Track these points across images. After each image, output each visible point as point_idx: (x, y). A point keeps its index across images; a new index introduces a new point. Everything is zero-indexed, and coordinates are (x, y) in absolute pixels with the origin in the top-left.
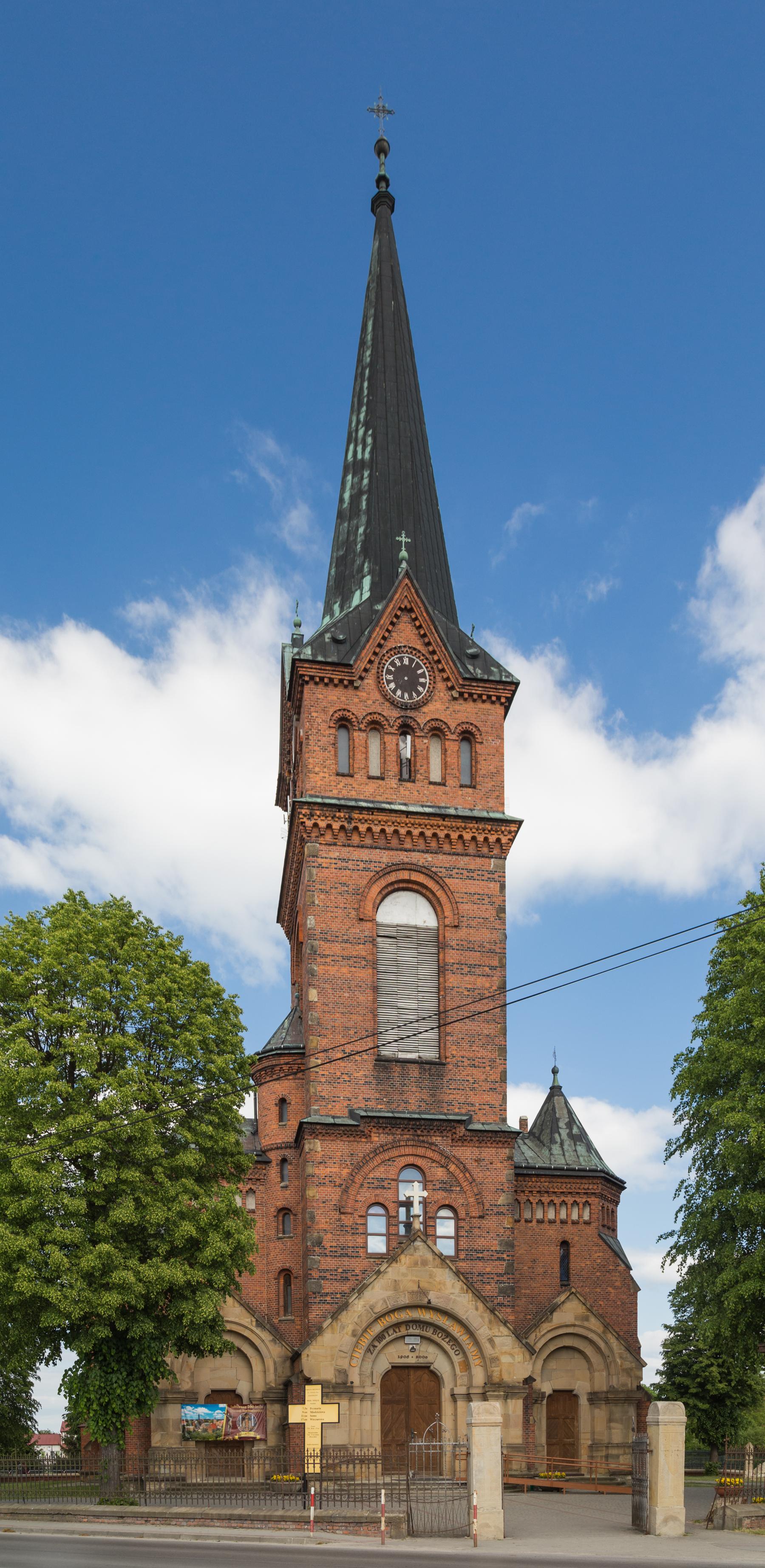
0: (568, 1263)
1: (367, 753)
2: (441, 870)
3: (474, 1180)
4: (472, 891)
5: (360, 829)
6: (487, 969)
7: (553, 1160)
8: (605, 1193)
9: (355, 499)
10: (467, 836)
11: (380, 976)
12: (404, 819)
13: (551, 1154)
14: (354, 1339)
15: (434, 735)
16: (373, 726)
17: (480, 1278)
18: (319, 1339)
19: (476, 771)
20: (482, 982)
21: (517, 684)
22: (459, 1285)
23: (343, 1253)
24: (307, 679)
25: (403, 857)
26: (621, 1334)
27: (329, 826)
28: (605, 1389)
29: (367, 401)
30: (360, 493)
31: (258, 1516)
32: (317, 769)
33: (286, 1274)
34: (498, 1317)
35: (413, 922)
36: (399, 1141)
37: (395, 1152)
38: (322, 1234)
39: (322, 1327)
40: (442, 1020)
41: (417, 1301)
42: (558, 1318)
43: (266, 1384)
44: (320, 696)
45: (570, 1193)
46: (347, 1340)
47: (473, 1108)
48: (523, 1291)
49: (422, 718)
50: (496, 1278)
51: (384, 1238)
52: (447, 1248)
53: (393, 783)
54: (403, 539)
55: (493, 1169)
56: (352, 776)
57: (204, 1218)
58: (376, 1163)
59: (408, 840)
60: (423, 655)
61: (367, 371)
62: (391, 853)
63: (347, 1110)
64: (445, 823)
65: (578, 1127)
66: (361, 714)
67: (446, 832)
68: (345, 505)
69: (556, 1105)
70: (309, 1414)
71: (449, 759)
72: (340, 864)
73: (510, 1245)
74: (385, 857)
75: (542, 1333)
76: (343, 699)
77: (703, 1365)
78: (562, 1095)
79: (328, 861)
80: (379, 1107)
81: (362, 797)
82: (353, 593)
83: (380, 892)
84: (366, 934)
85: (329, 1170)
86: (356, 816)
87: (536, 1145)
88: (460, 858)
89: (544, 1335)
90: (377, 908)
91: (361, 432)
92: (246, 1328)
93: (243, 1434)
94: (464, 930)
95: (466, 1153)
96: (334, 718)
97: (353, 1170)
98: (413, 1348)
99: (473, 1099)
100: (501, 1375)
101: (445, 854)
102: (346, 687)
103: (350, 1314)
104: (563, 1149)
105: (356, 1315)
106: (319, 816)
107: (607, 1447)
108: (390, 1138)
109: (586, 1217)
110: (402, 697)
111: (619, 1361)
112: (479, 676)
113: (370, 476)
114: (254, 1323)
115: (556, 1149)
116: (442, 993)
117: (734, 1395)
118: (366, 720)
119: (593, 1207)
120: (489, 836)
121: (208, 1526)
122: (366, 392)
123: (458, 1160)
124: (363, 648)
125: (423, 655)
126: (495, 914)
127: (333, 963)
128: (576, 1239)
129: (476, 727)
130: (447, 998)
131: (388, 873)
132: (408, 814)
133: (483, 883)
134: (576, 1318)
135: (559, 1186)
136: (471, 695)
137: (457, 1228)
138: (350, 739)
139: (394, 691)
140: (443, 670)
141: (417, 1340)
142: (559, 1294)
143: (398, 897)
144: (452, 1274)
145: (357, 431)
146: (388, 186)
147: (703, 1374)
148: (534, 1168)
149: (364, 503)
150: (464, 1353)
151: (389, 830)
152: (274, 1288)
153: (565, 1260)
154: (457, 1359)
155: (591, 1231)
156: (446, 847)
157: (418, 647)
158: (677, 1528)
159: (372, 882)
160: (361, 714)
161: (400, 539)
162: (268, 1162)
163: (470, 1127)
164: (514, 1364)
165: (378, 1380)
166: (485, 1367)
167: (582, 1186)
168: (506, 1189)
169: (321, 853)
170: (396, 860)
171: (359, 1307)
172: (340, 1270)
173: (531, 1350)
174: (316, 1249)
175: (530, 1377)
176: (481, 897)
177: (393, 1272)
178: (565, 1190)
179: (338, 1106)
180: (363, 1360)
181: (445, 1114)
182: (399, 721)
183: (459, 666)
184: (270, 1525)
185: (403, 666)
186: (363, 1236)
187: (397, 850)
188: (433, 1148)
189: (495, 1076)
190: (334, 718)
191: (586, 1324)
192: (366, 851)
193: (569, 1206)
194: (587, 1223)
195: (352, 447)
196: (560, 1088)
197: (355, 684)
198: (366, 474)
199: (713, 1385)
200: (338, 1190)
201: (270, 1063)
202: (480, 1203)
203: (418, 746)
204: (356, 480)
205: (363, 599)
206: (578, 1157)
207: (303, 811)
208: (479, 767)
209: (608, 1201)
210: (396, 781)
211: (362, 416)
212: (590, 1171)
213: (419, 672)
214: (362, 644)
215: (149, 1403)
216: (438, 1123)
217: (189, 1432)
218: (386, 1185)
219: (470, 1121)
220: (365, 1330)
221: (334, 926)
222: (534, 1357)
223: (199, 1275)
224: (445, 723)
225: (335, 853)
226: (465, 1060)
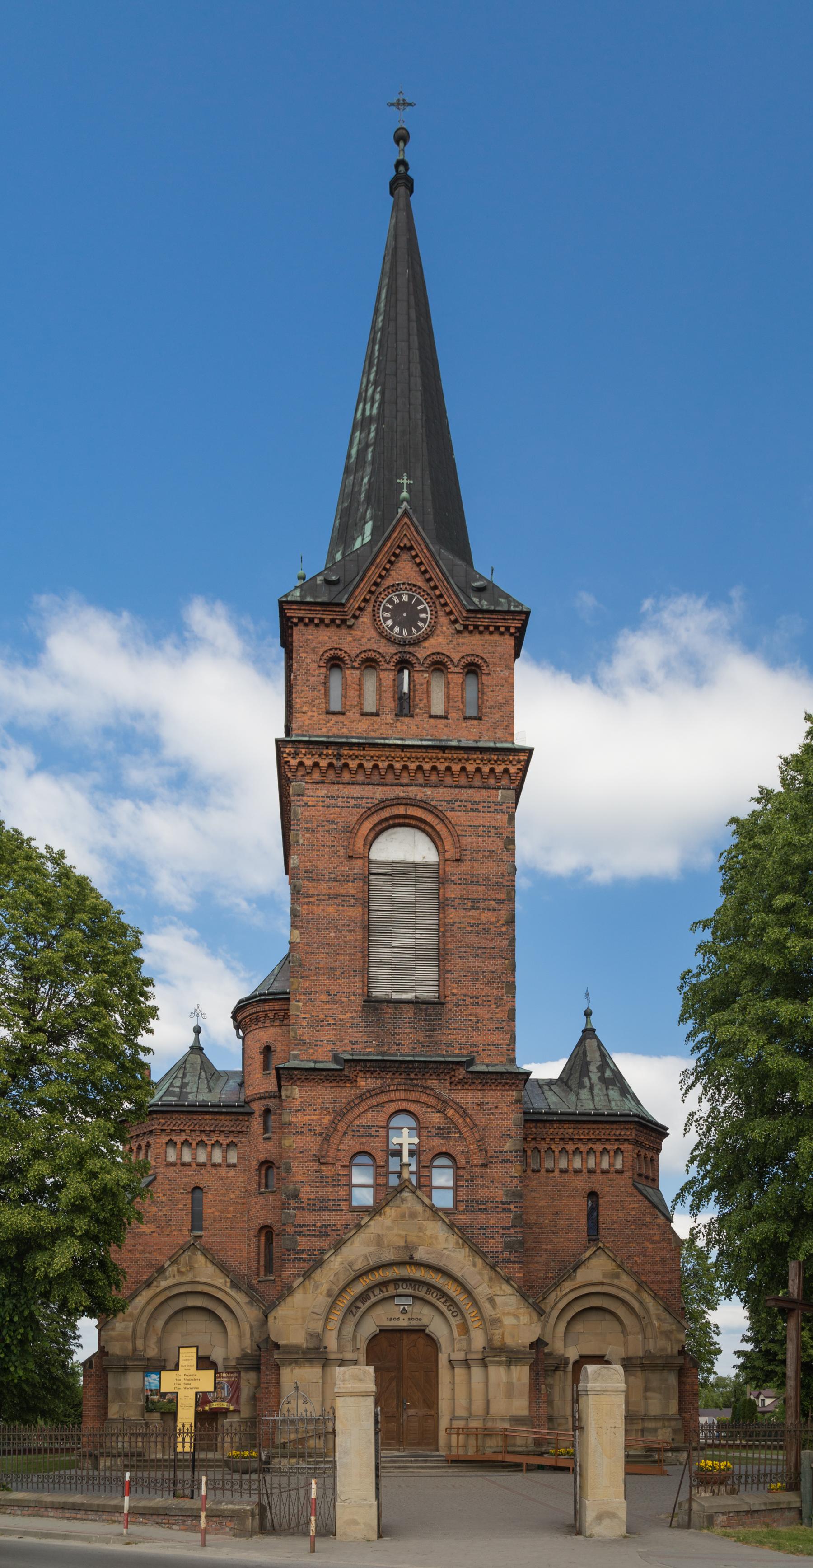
0: (598, 1215)
1: (361, 690)
2: (441, 803)
3: (476, 1125)
4: (477, 823)
5: (351, 766)
6: (493, 903)
7: (579, 1104)
8: (641, 1139)
9: (362, 453)
10: (471, 768)
12: (399, 753)
13: (578, 1099)
14: (330, 1300)
15: (436, 670)
16: (368, 663)
17: (482, 1232)
18: (289, 1299)
19: (483, 703)
20: (486, 916)
21: (527, 614)
22: (453, 1239)
23: (321, 1206)
24: (295, 620)
25: (399, 792)
26: (661, 1292)
27: (316, 765)
29: (378, 362)
30: (367, 446)
31: (91, 1505)
32: (305, 709)
33: (267, 1231)
34: (500, 1274)
35: (410, 858)
36: (389, 1085)
37: (384, 1098)
39: (291, 1287)
40: (441, 957)
42: (582, 1276)
43: (243, 1350)
44: (310, 637)
45: (599, 1140)
48: (544, 1247)
51: (372, 1189)
52: (443, 1200)
53: (390, 718)
54: (405, 481)
55: (500, 1115)
57: (64, 1155)
58: (362, 1110)
60: (424, 591)
61: (379, 335)
62: (386, 788)
63: (330, 1054)
64: (445, 755)
65: (612, 1070)
67: (446, 764)
68: (352, 460)
69: (588, 1048)
71: (451, 692)
72: (328, 802)
73: (518, 1195)
74: (379, 793)
75: (564, 1292)
78: (596, 1038)
80: (368, 1050)
81: (354, 734)
84: (356, 871)
85: (307, 1117)
86: (346, 752)
89: (566, 1295)
91: (370, 391)
92: (220, 1289)
93: (215, 1405)
94: (467, 863)
95: (467, 1097)
96: (325, 657)
97: (335, 1118)
98: (404, 1309)
100: (503, 1338)
101: (445, 787)
102: (338, 626)
103: (325, 1272)
104: (592, 1093)
106: (305, 755)
108: (379, 1083)
112: (485, 608)
113: (377, 429)
114: (229, 1284)
116: (441, 930)
118: (360, 658)
120: (495, 766)
121: (42, 1516)
122: (376, 354)
123: (457, 1104)
125: (424, 591)
126: (502, 845)
127: (318, 902)
129: (482, 658)
130: (447, 935)
131: (382, 809)
132: (403, 747)
133: (489, 815)
134: (604, 1276)
135: (584, 1133)
137: (456, 1178)
138: (344, 678)
141: (410, 1300)
143: (394, 833)
144: (445, 1228)
145: (366, 390)
146: (407, 169)
148: (556, 1114)
150: (462, 1314)
151: (383, 765)
152: (254, 1247)
153: (593, 1214)
154: (454, 1321)
155: (625, 1180)
156: (448, 780)
157: (419, 584)
158: (614, 1528)
159: (363, 819)
161: (401, 481)
162: (251, 1114)
163: (471, 1069)
164: (518, 1325)
165: (362, 1345)
166: (485, 1329)
167: (613, 1132)
168: (513, 1134)
169: (307, 791)
170: (390, 796)
171: (336, 1266)
172: (319, 1225)
173: (541, 1313)
174: (292, 1202)
175: (539, 1340)
176: (487, 829)
177: (375, 1226)
178: (592, 1137)
179: (321, 1050)
180: (342, 1323)
181: (444, 1056)
182: (397, 657)
183: (462, 598)
184: (104, 1517)
185: (402, 602)
186: (346, 1188)
187: (392, 785)
189: (501, 1014)
190: (325, 657)
191: (616, 1282)
192: (358, 787)
193: (598, 1154)
194: (619, 1172)
195: (361, 406)
196: (594, 1030)
198: (373, 428)
201: (254, 1010)
204: (363, 435)
205: (365, 542)
206: (610, 1101)
207: (287, 750)
208: (485, 698)
209: (644, 1147)
210: (393, 716)
211: (372, 377)
212: (622, 1115)
213: (420, 607)
215: (12, 1369)
216: (434, 1065)
217: (153, 1403)
219: (471, 1062)
221: (321, 865)
222: (542, 1318)
223: (49, 1222)
224: (448, 657)
225: (323, 791)
226: (467, 998)
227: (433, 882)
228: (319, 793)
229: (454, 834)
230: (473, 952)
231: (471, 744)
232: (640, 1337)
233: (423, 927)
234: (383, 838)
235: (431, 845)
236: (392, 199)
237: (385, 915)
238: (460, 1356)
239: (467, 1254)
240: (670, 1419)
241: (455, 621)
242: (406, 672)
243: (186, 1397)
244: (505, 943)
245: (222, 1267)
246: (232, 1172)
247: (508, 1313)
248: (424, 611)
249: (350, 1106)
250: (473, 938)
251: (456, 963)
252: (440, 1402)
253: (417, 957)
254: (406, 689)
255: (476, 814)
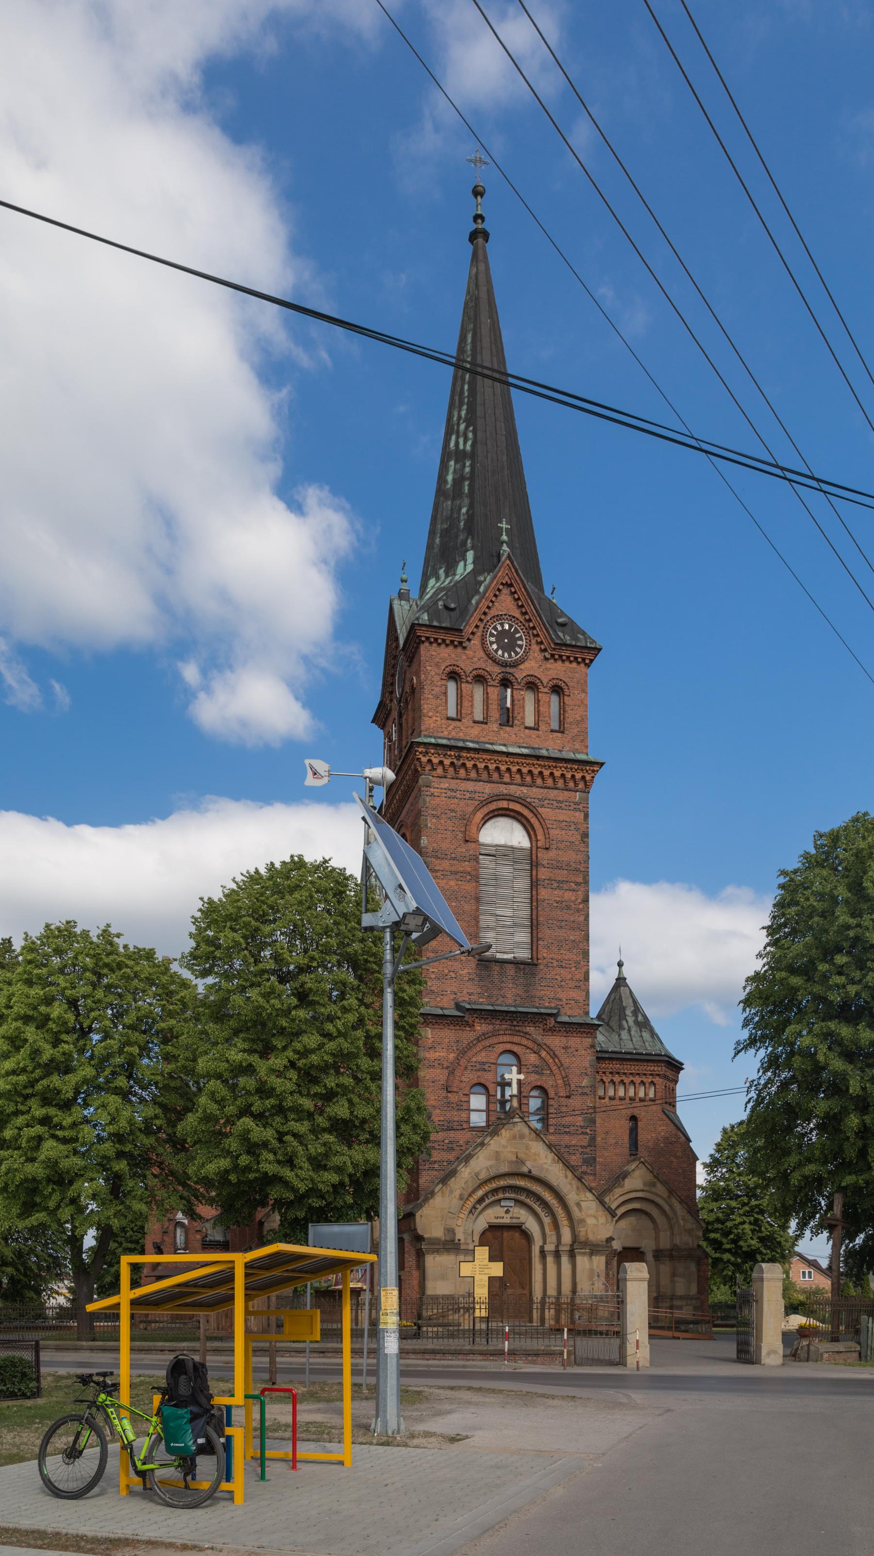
1: (472, 701)
3: (562, 1065)
4: (561, 819)
6: (573, 885)
7: (622, 1044)
9: (458, 482)
10: (557, 774)
11: (481, 888)
14: (461, 1202)
17: (567, 1150)
18: (431, 1201)
19: (564, 719)
22: (551, 1156)
24: (423, 639)
26: (683, 1198)
27: (441, 762)
28: (668, 1247)
29: (468, 401)
32: (430, 714)
36: (498, 1030)
37: (494, 1040)
40: (534, 926)
41: (514, 1169)
44: (434, 653)
45: (638, 1074)
46: (456, 1202)
47: (561, 1003)
49: (520, 673)
53: (495, 727)
54: (504, 525)
55: (578, 1055)
56: (460, 720)
58: (478, 1049)
59: (507, 775)
62: (493, 785)
63: (453, 1003)
66: (468, 669)
67: (539, 769)
69: (623, 995)
71: (541, 709)
74: (488, 789)
76: (453, 656)
77: (736, 1222)
78: (628, 986)
79: (439, 790)
82: (457, 563)
83: (483, 818)
84: (471, 853)
85: (438, 1054)
86: (464, 755)
88: (550, 791)
90: (479, 829)
91: (462, 427)
95: (556, 1042)
97: (458, 1055)
105: (463, 1181)
107: (672, 1299)
108: (491, 1027)
109: (651, 1095)
110: (503, 656)
111: (682, 1222)
112: (568, 642)
115: (624, 1035)
117: (764, 1251)
119: (657, 1086)
122: (466, 394)
123: (549, 1047)
124: (472, 616)
126: (579, 838)
128: (643, 1114)
132: (508, 754)
133: (570, 812)
134: (645, 1185)
135: (628, 1068)
136: (561, 656)
139: (496, 651)
140: (538, 635)
144: (545, 1147)
145: (458, 425)
147: (735, 1231)
149: (466, 488)
160: (468, 669)
163: (558, 1020)
168: (589, 1073)
170: (496, 792)
171: (465, 1173)
172: (447, 1141)
177: (495, 1144)
179: (445, 999)
181: (537, 1008)
185: (504, 630)
186: (467, 1112)
189: (580, 976)
191: (653, 1189)
192: (472, 783)
195: (454, 437)
196: (625, 979)
198: (468, 463)
199: (746, 1241)
200: (446, 1072)
202: (567, 1084)
203: (515, 697)
204: (458, 466)
207: (420, 750)
210: (497, 725)
211: (463, 413)
212: (655, 1055)
213: (517, 635)
214: (470, 613)
218: (487, 1068)
220: (470, 1195)
221: (444, 846)
226: (554, 961)
227: (527, 864)
228: (442, 786)
229: (545, 827)
230: (558, 924)
231: (557, 755)
233: (519, 900)
234: (488, 825)
235: (524, 833)
236: (471, 247)
237: (491, 889)
240: (692, 1299)
241: (545, 650)
242: (509, 691)
243: (481, 1280)
244: (582, 918)
247: (591, 1215)
248: (520, 638)
249: (470, 1046)
250: (559, 913)
251: (545, 932)
253: (515, 925)
254: (509, 705)
255: (560, 811)
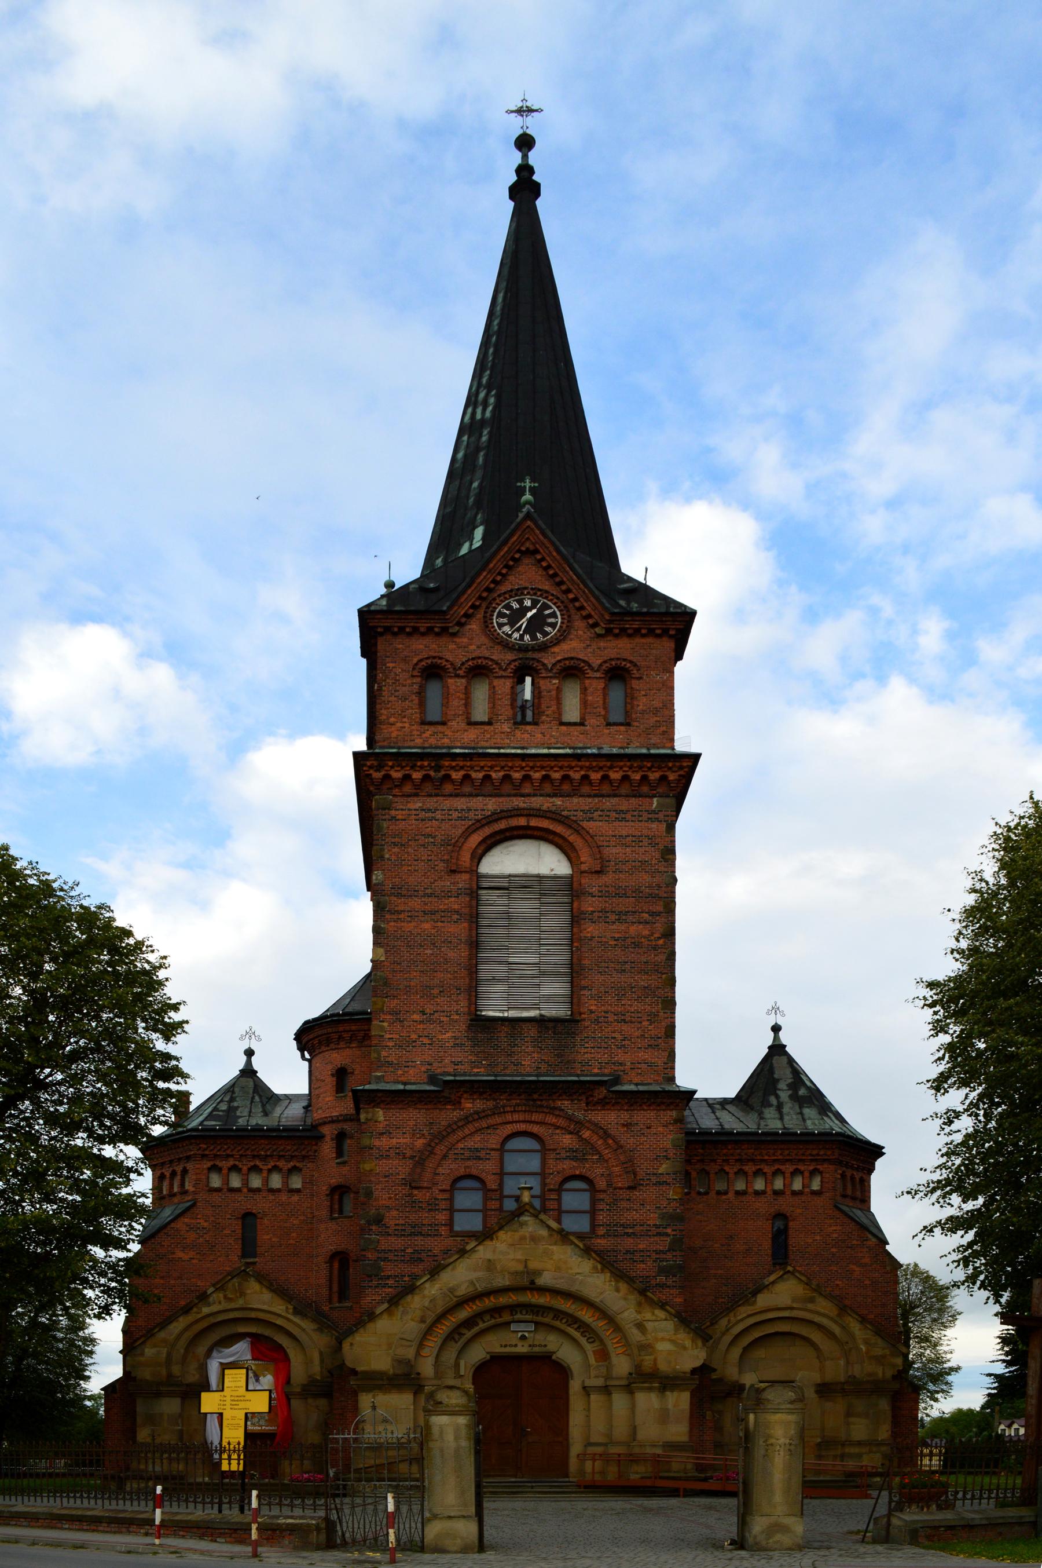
0: (786, 1239)
4: (624, 833)
6: (646, 915)
7: (762, 1123)
11: (482, 931)
12: (518, 763)
17: (628, 1256)
25: (519, 802)
30: (478, 449)
32: (392, 720)
36: (504, 1107)
38: (382, 1211)
40: (575, 972)
42: (763, 1300)
47: (622, 1068)
50: (654, 1256)
53: (506, 727)
54: (528, 484)
58: (467, 1131)
61: (494, 338)
70: (228, 1403)
74: (491, 805)
75: (739, 1318)
80: (476, 1070)
85: (394, 1140)
86: (447, 763)
87: (743, 1110)
94: (611, 875)
95: (611, 1118)
96: (420, 666)
97: (431, 1140)
99: (620, 1057)
107: (843, 1445)
108: (491, 1104)
109: (816, 1185)
114: (291, 1311)
126: (658, 855)
134: (794, 1300)
137: (594, 1202)
140: (582, 608)
142: (770, 1273)
159: (468, 833)
167: (809, 1152)
171: (433, 1292)
172: (409, 1250)
177: (484, 1252)
181: (578, 1076)
183: (604, 601)
188: (557, 1113)
191: (810, 1306)
192: (463, 799)
197: (451, 631)
198: (485, 432)
204: (473, 439)
206: (804, 1120)
207: (368, 763)
232: (842, 1362)
238: (600, 1382)
239: (608, 1278)
244: (662, 957)
245: (281, 1292)
246: (295, 1198)
252: (571, 1429)
253: (543, 974)
